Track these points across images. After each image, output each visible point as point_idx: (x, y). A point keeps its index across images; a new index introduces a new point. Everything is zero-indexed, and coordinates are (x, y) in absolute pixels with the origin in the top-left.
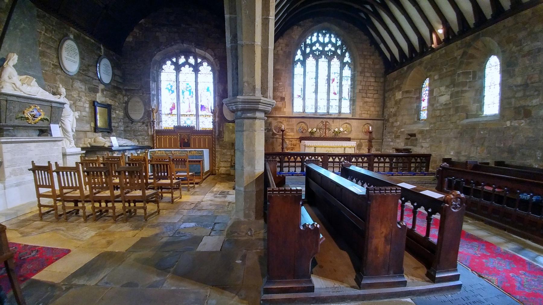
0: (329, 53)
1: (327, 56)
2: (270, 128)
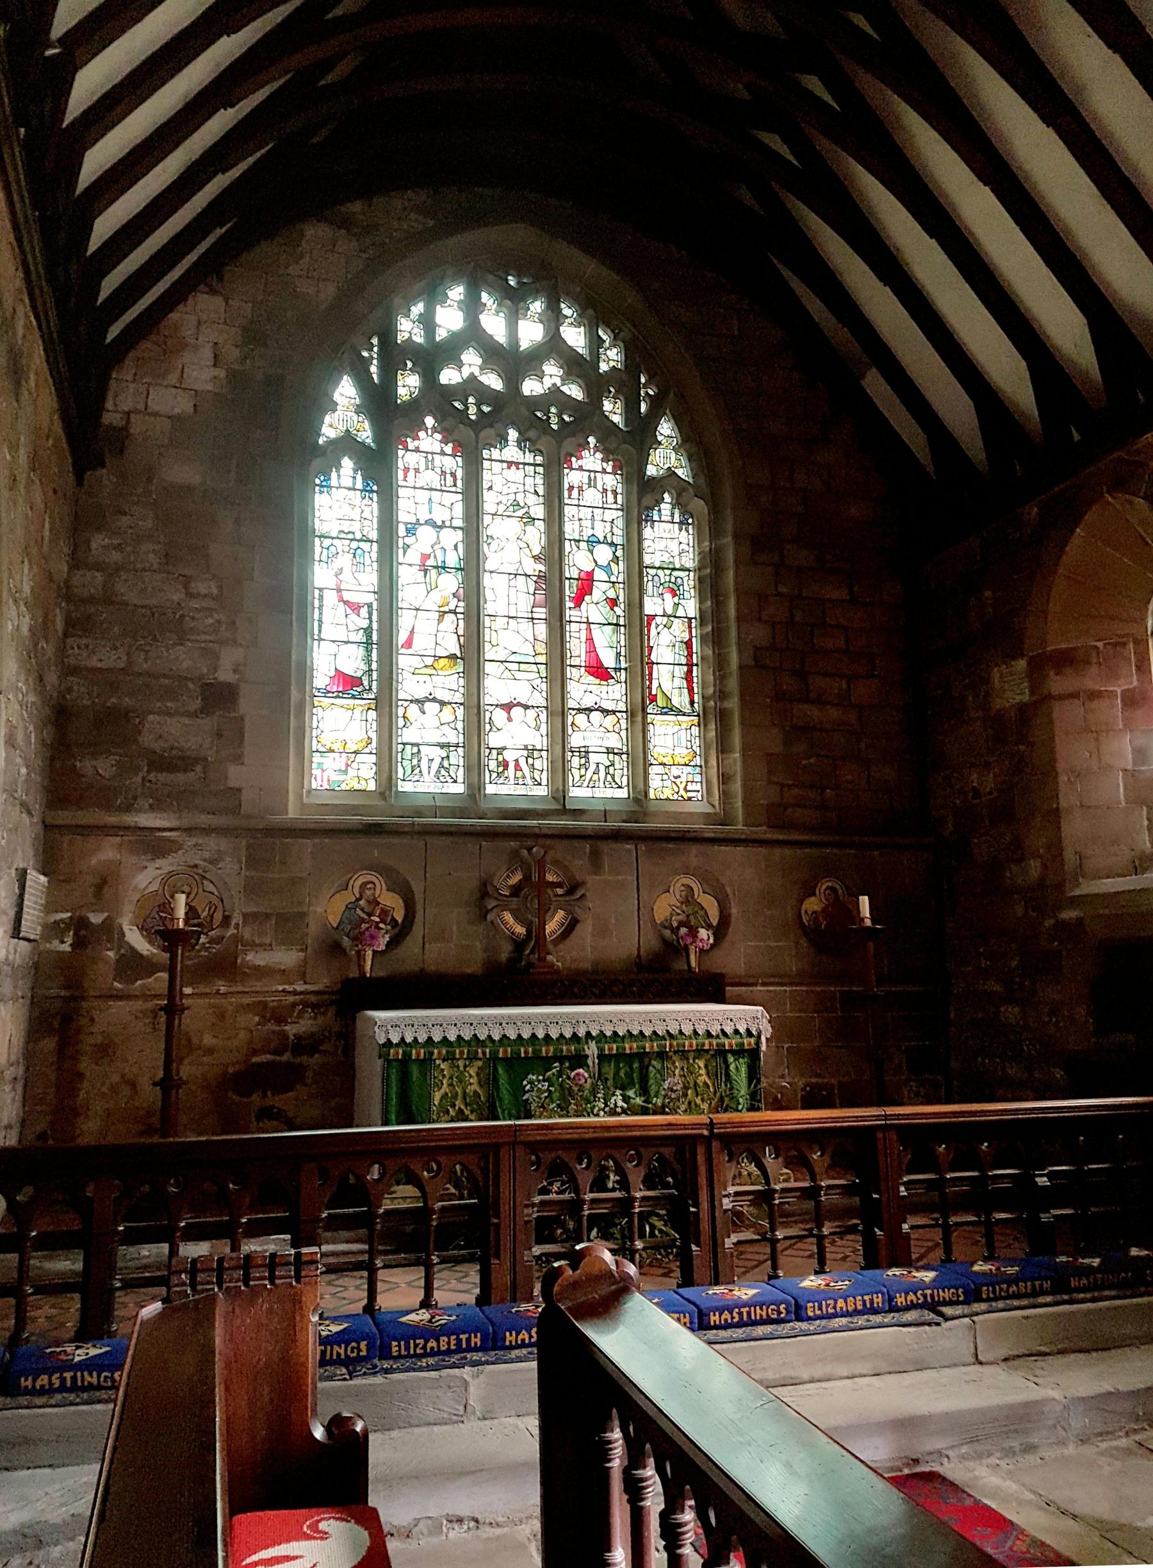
2: (96, 919)
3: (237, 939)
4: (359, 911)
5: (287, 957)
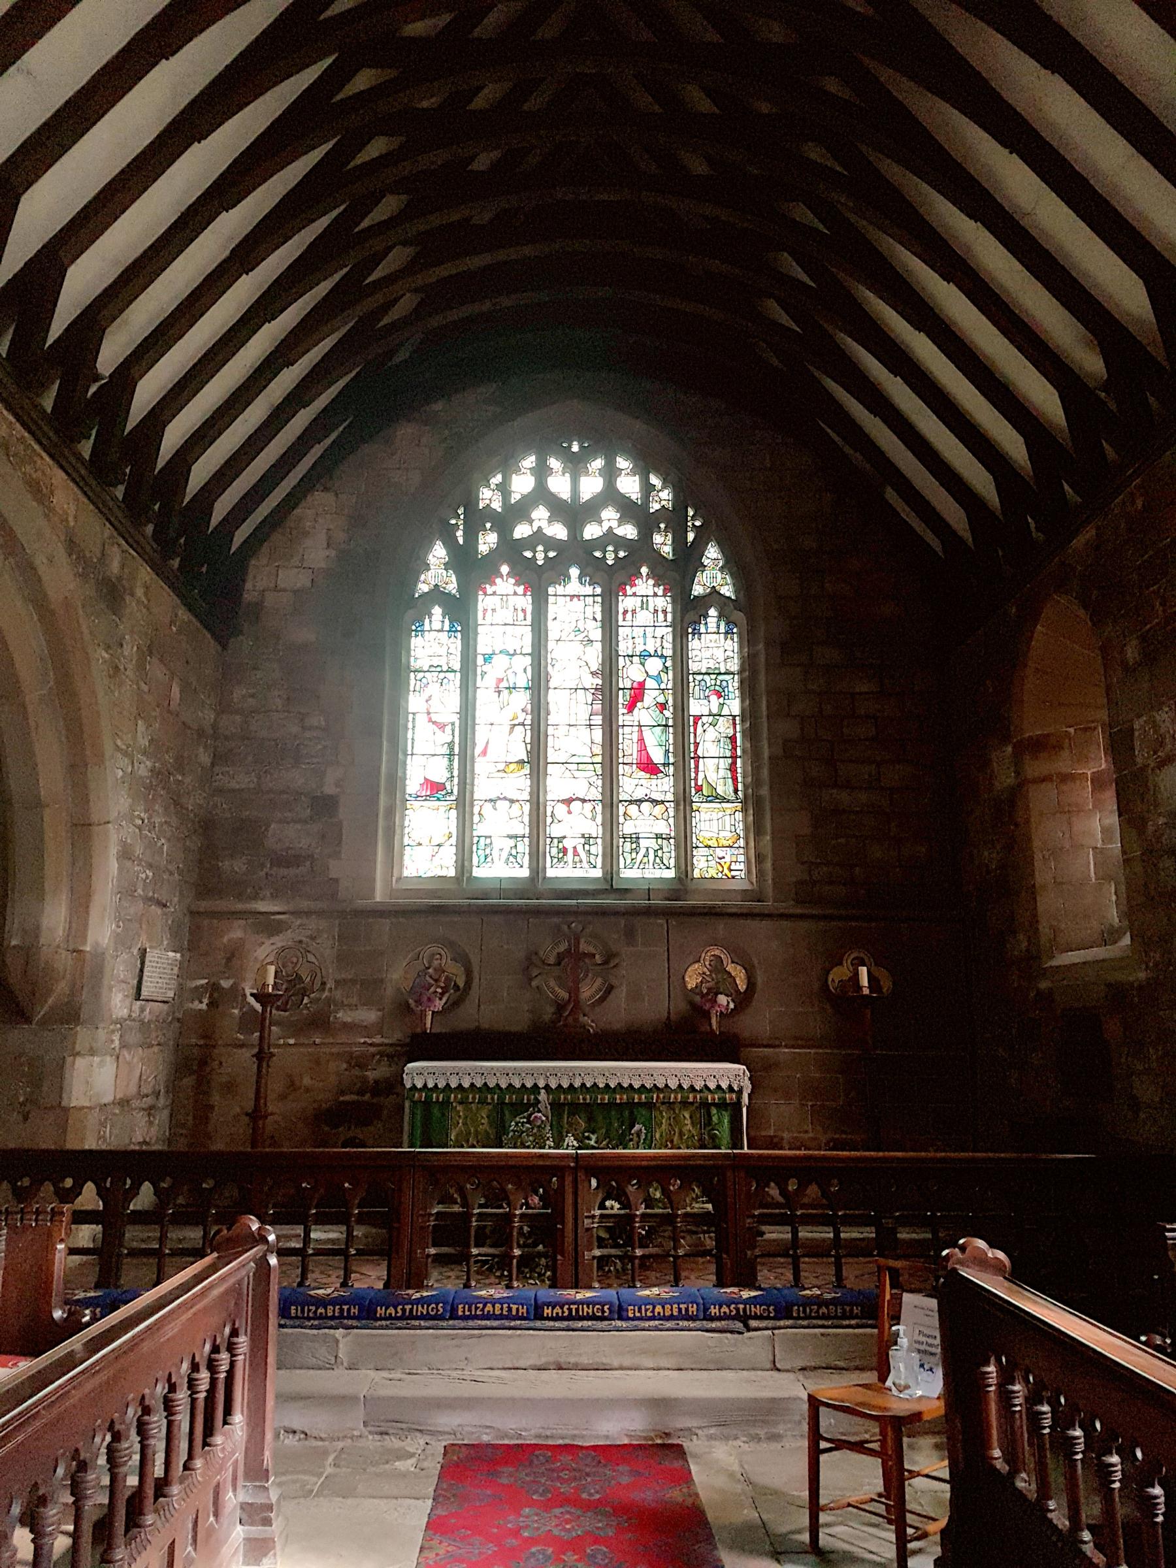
0: (540, 556)
1: (594, 569)
2: (226, 984)
3: (329, 1001)
4: (428, 978)
5: (369, 1016)
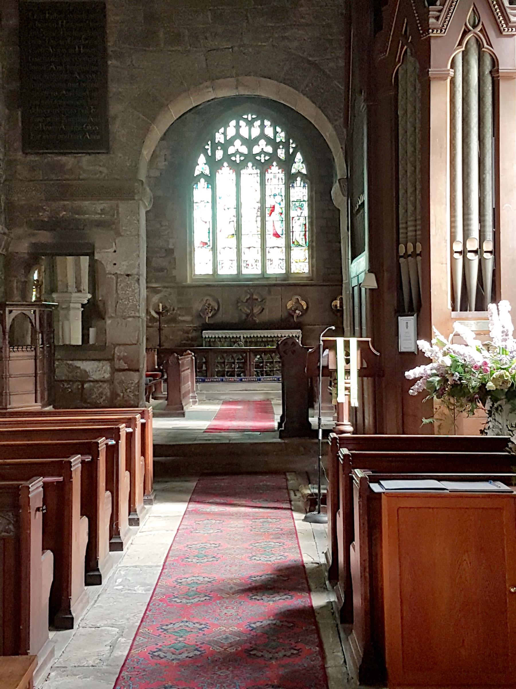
5: (188, 318)
